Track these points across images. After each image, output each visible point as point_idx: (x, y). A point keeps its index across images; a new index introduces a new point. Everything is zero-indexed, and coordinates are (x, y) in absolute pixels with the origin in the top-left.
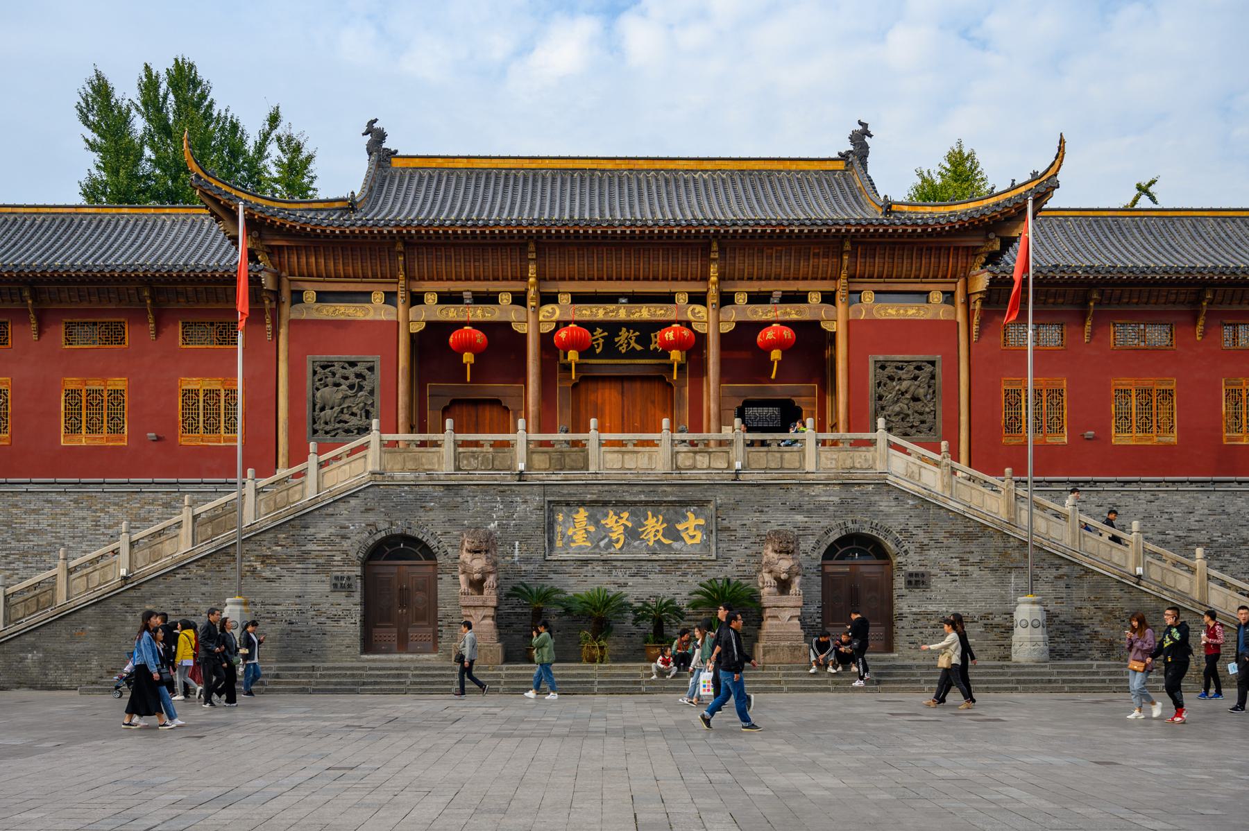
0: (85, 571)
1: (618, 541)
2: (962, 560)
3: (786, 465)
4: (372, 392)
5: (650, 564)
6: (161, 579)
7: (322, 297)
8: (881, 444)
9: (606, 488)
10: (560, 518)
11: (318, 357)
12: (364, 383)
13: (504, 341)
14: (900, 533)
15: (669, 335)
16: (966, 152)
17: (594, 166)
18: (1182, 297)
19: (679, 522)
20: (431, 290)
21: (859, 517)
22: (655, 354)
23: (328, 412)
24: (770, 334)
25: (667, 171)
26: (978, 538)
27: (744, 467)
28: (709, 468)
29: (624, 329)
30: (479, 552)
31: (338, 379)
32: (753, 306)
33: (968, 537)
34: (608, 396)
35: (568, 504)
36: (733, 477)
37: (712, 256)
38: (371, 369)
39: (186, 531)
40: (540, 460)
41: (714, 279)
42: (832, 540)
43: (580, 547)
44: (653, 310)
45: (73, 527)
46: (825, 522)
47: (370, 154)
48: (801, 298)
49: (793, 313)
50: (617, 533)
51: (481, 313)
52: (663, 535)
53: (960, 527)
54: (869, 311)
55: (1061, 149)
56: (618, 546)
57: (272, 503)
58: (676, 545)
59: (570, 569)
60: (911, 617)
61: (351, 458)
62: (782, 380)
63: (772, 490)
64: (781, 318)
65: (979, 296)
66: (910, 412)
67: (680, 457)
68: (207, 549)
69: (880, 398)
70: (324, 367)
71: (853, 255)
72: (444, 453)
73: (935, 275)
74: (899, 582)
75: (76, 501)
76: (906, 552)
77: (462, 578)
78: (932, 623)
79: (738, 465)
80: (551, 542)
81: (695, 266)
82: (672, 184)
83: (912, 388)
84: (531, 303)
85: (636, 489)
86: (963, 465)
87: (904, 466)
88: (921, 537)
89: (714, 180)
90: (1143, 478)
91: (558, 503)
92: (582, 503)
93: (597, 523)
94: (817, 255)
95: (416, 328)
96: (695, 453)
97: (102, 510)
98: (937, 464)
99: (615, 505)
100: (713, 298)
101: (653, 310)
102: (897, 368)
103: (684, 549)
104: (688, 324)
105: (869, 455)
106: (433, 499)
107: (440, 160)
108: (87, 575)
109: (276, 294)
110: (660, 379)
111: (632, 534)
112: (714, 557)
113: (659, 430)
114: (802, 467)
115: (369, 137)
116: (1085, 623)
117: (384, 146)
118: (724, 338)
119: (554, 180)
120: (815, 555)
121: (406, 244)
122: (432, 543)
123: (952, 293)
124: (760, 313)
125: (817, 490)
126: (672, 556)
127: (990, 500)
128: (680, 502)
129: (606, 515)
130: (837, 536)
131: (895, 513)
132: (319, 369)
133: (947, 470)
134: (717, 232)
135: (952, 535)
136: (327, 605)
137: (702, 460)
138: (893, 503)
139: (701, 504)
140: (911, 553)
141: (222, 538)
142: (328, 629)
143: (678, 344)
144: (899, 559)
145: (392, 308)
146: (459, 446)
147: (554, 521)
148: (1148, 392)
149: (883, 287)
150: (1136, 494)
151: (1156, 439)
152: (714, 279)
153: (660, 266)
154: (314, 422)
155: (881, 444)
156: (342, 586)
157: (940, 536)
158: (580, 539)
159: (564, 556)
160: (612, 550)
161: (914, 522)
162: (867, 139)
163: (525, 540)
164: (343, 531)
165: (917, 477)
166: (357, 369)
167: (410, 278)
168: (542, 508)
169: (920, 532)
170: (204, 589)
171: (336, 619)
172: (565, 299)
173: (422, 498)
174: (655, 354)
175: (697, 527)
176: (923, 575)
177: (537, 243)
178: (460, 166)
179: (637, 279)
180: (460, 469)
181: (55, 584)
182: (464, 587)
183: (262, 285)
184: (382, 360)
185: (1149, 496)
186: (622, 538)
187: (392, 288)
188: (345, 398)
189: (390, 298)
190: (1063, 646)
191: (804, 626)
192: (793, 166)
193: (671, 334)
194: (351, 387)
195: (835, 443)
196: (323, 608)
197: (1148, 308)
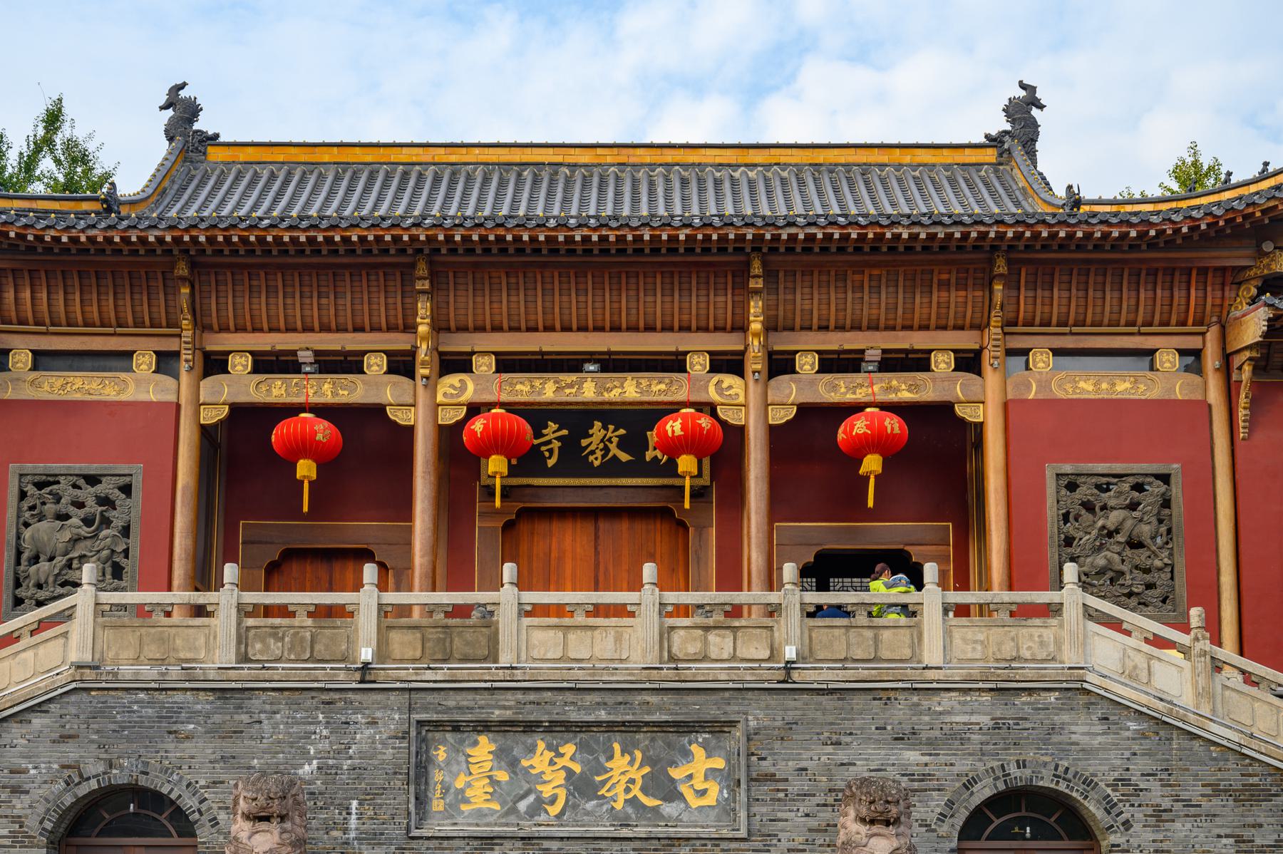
3: (885, 654)
4: (126, 531)
7: (41, 359)
8: (1072, 613)
9: (532, 697)
10: (441, 754)
11: (29, 467)
12: (112, 514)
13: (370, 445)
14: (1114, 786)
15: (674, 427)
16: (1206, 162)
17: (559, 159)
19: (673, 763)
20: (240, 347)
21: (1030, 755)
22: (654, 469)
23: (44, 566)
24: (859, 426)
25: (685, 166)
26: (1270, 796)
27: (801, 657)
28: (733, 658)
29: (598, 424)
30: (267, 819)
32: (828, 377)
34: (571, 541)
35: (456, 727)
36: (780, 675)
37: (753, 284)
38: (126, 490)
41: (756, 326)
42: (977, 800)
43: (480, 813)
44: (644, 383)
46: (964, 765)
48: (917, 362)
49: (904, 389)
50: (553, 784)
51: (329, 390)
52: (644, 790)
53: (1232, 776)
56: (554, 810)
58: (669, 809)
62: (889, 498)
63: (858, 701)
64: (881, 398)
65: (1247, 354)
66: (1124, 568)
67: (677, 637)
69: (1069, 541)
70: (40, 486)
71: (1012, 283)
72: (217, 629)
73: (1164, 323)
76: (1127, 824)
79: (790, 652)
80: (422, 801)
81: (722, 303)
82: (694, 186)
83: (1129, 524)
84: (422, 371)
85: (589, 699)
86: (1227, 651)
87: (1117, 656)
88: (1156, 794)
89: (766, 180)
91: (437, 725)
92: (484, 727)
93: (513, 765)
95: (212, 416)
96: (707, 629)
99: (549, 730)
100: (755, 362)
101: (644, 383)
102: (1098, 487)
103: (685, 817)
104: (711, 409)
105: (1048, 634)
106: (193, 716)
107: (292, 150)
110: (664, 514)
111: (583, 786)
112: (743, 833)
113: (636, 585)
114: (915, 656)
115: (170, 112)
117: (196, 126)
118: (775, 434)
119: (486, 180)
120: (944, 829)
121: (193, 265)
122: (189, 803)
123: (1197, 353)
124: (841, 389)
125: (946, 701)
126: (660, 831)
128: (676, 724)
129: (531, 750)
130: (988, 793)
131: (1103, 748)
132: (30, 489)
133: (1203, 664)
134: (759, 238)
135: (1216, 790)
137: (720, 644)
138: (1099, 728)
139: (719, 728)
140: (1137, 827)
143: (692, 442)
144: (1113, 839)
145: (168, 381)
146: (248, 615)
147: (430, 760)
149: (1069, 342)
152: (756, 326)
153: (657, 304)
154: (18, 584)
155: (1072, 613)
157: (1194, 792)
158: (479, 796)
159: (448, 829)
160: (542, 818)
161: (1141, 765)
162: (1035, 112)
163: (370, 797)
164: (15, 780)
165: (1143, 676)
166: (100, 489)
167: (202, 326)
168: (405, 736)
169: (1154, 785)
172: (484, 365)
173: (170, 716)
174: (654, 469)
175: (710, 774)
177: (431, 264)
178: (326, 159)
179: (616, 328)
186: (562, 794)
187: (172, 345)
188: (76, 540)
189: (166, 362)
192: (907, 158)
193: (677, 426)
194: (88, 522)
195: (984, 610)
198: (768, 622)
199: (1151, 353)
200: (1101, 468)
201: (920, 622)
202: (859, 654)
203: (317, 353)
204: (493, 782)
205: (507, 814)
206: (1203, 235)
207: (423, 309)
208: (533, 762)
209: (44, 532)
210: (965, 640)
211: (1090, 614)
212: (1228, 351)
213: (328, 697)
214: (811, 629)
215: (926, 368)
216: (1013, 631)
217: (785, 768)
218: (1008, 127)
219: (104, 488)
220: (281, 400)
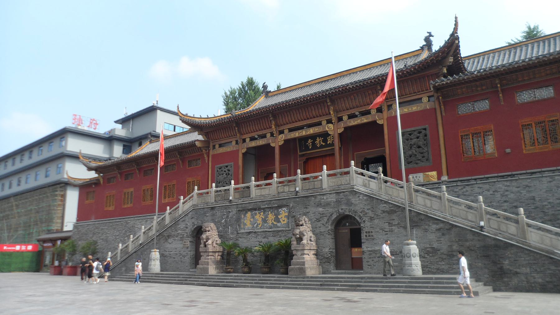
2: (389, 223)
3: (316, 187)
7: (220, 146)
14: (361, 212)
20: (247, 137)
26: (395, 212)
33: (391, 212)
46: (331, 210)
50: (260, 221)
53: (387, 207)
55: (456, 25)
56: (260, 226)
58: (279, 224)
59: (245, 236)
60: (368, 253)
76: (364, 221)
88: (371, 214)
90: (543, 169)
93: (253, 218)
96: (284, 186)
99: (258, 210)
100: (334, 120)
105: (348, 178)
111: (265, 221)
130: (335, 216)
139: (287, 206)
140: (366, 222)
150: (541, 179)
151: (551, 147)
161: (366, 207)
162: (431, 38)
167: (241, 134)
171: (184, 256)
172: (286, 131)
175: (285, 216)
190: (443, 267)
196: (182, 252)
200: (409, 129)
203: (359, 112)
204: (251, 221)
211: (357, 172)
213: (226, 207)
220: (360, 123)
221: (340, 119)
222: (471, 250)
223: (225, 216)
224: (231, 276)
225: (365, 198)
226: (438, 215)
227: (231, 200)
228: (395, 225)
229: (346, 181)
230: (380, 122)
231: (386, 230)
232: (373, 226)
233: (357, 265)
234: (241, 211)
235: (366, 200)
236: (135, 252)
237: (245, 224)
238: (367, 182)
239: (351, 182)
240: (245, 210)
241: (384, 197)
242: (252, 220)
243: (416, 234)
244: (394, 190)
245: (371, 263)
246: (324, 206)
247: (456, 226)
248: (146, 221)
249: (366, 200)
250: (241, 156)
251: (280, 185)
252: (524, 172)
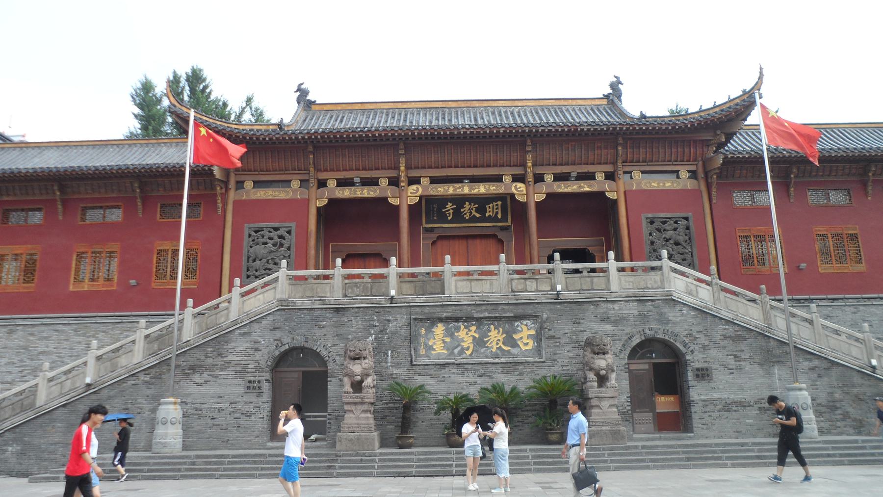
0: (60, 381)
1: (468, 349)
2: (735, 356)
4: (289, 249)
5: (494, 366)
6: (116, 385)
9: (458, 308)
11: (252, 225)
12: (283, 241)
14: (686, 337)
18: (853, 171)
21: (654, 326)
23: (258, 262)
26: (745, 339)
27: (563, 290)
29: (467, 203)
31: (265, 240)
36: (555, 297)
38: (289, 232)
39: (140, 345)
40: (407, 288)
45: (72, 349)
46: (628, 330)
47: (299, 103)
53: (731, 331)
54: (638, 184)
55: (761, 78)
56: (468, 353)
57: (204, 325)
58: (515, 351)
59: (432, 372)
60: (701, 404)
61: (264, 290)
62: (587, 227)
67: (514, 283)
68: (153, 361)
69: (652, 243)
70: (256, 232)
71: (625, 147)
73: (682, 161)
74: (690, 375)
75: (75, 331)
76: (692, 352)
77: (346, 380)
78: (718, 407)
81: (515, 156)
88: (703, 339)
90: (847, 296)
92: (441, 320)
93: (451, 335)
94: (600, 148)
96: (525, 279)
97: (93, 336)
98: (708, 284)
99: (465, 321)
105: (658, 278)
108: (61, 383)
109: (226, 183)
111: (480, 342)
113: (497, 262)
115: (298, 93)
116: (838, 405)
120: (622, 356)
121: (314, 147)
122: (324, 353)
127: (748, 310)
130: (638, 341)
134: (530, 131)
136: (242, 404)
137: (531, 285)
139: (534, 317)
140: (696, 353)
141: (164, 354)
142: (242, 422)
148: (838, 237)
152: (530, 164)
153: (491, 157)
154: (248, 270)
156: (254, 388)
157: (718, 338)
159: (427, 361)
160: (464, 355)
161: (695, 329)
162: (620, 86)
164: (257, 346)
166: (279, 232)
167: (318, 170)
169: (701, 336)
170: (149, 392)
171: (248, 414)
172: (425, 181)
175: (529, 336)
176: (707, 369)
177: (405, 144)
179: (475, 166)
180: (346, 296)
181: (36, 391)
182: (348, 388)
183: (214, 176)
184: (297, 226)
185: (852, 309)
186: (471, 346)
187: (305, 177)
189: (304, 183)
191: (620, 413)
194: (274, 245)
196: (239, 405)
197: (831, 179)
198: (550, 276)
199: (677, 172)
200: (662, 215)
201: (608, 275)
202: (585, 288)
203: (361, 179)
204: (444, 342)
205: (449, 355)
206: (689, 129)
207: (403, 161)
208: (460, 333)
209: (260, 250)
210: (626, 281)
211: (674, 270)
212: (709, 169)
213: (378, 310)
214: (566, 278)
215: (594, 179)
216: (644, 277)
217: (558, 334)
218: (611, 91)
219: (282, 232)
220: (578, 191)
221: (539, 179)
222: (861, 400)
223: (377, 329)
224: (412, 453)
225: (693, 313)
226: (812, 347)
227: (392, 297)
228: (745, 360)
229: (655, 282)
230: (612, 196)
231: (731, 367)
232: (708, 359)
233: (678, 421)
234: (421, 320)
235: (695, 317)
236: (64, 406)
237: (431, 348)
238: (693, 287)
239: (666, 285)
240: (432, 321)
241: (724, 314)
242: (448, 340)
243: (780, 375)
244: (740, 305)
245: (707, 419)
246: (616, 321)
247: (838, 363)
248: (11, 332)
249: (695, 317)
250: (313, 213)
251: (517, 277)
252: (824, 297)
